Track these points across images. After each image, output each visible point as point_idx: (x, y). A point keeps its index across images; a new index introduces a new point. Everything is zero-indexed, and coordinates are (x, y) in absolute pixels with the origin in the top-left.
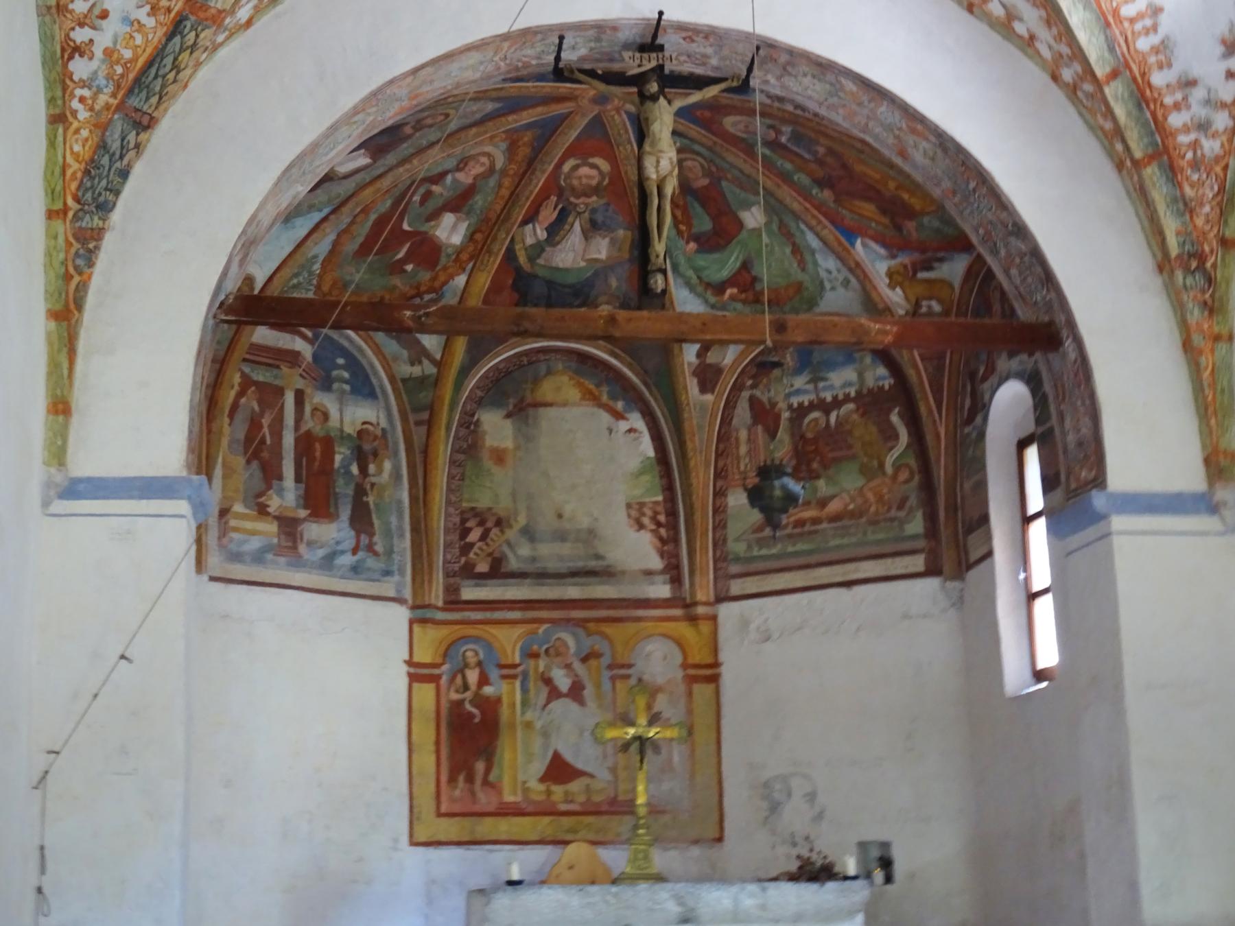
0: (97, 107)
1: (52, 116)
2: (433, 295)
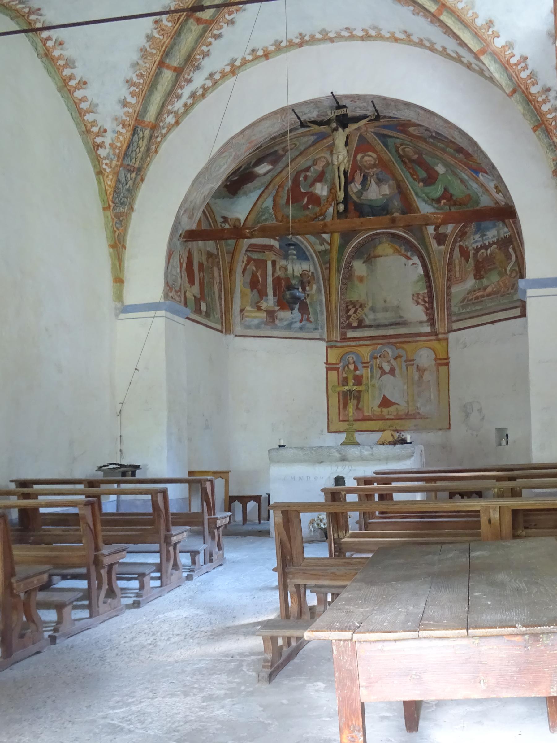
0: (113, 167)
1: (97, 172)
2: (322, 217)
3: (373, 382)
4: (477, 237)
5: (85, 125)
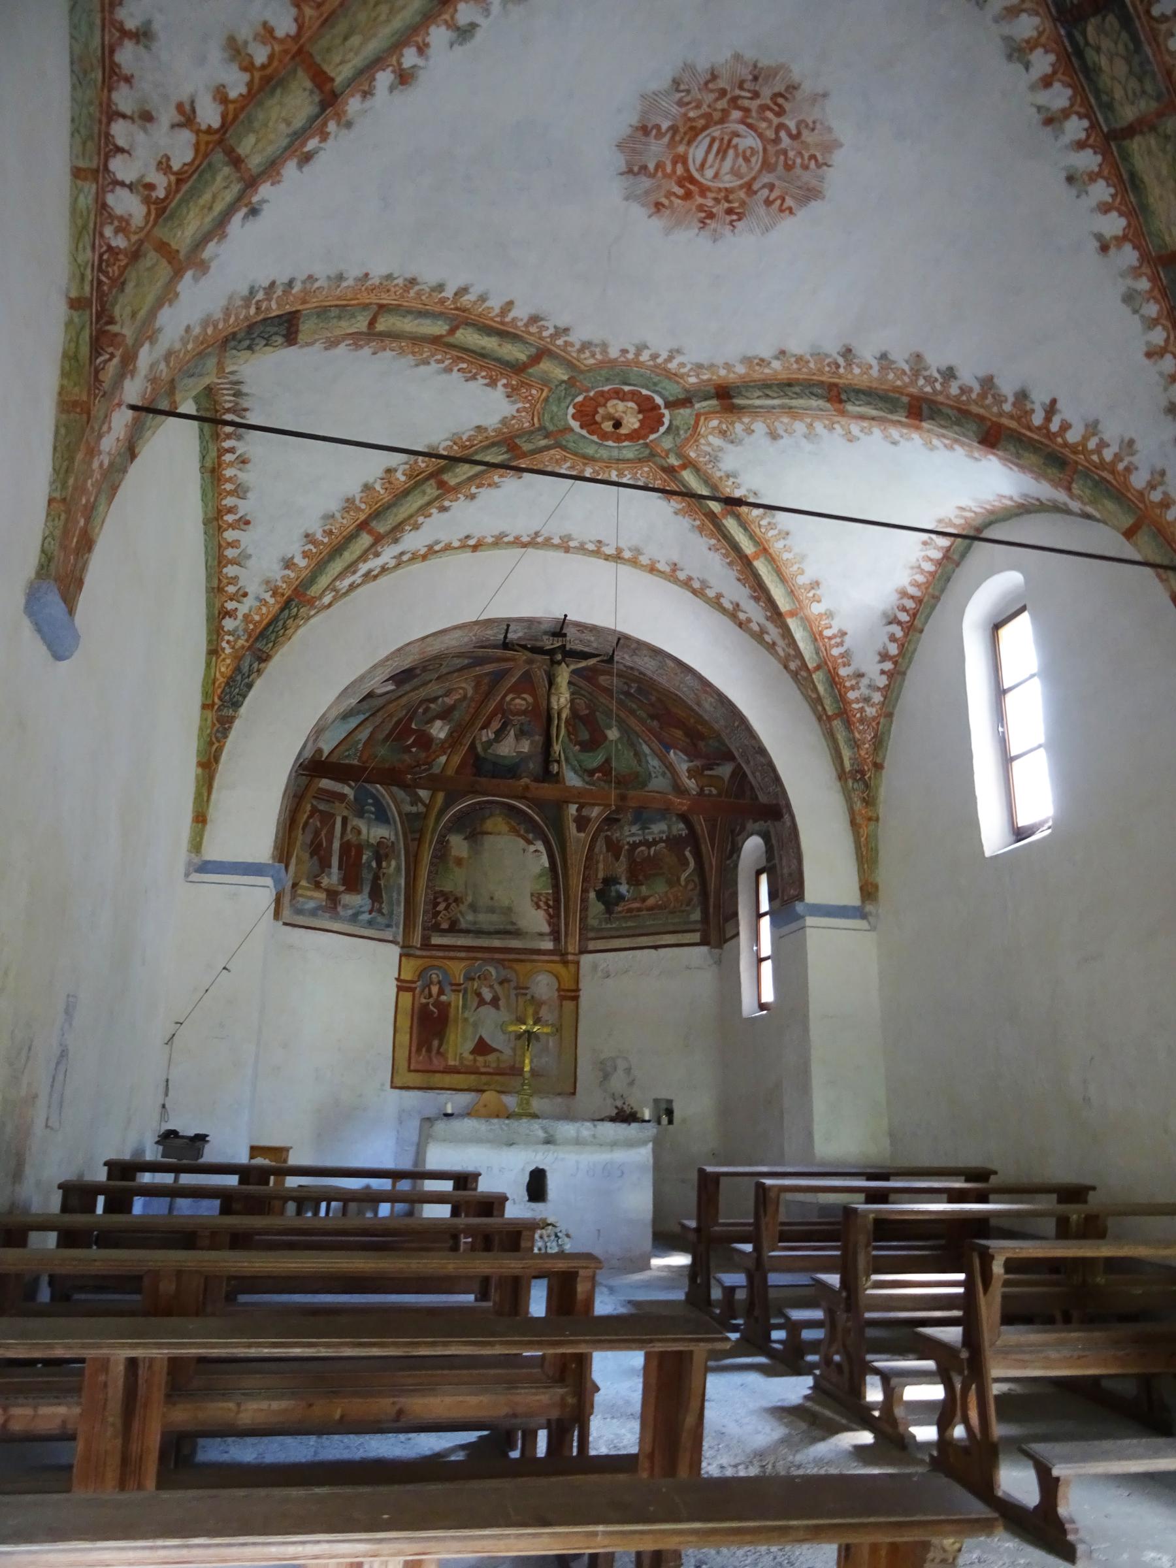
0: (237, 647)
3: (466, 1015)
4: (634, 829)
5: (219, 579)
